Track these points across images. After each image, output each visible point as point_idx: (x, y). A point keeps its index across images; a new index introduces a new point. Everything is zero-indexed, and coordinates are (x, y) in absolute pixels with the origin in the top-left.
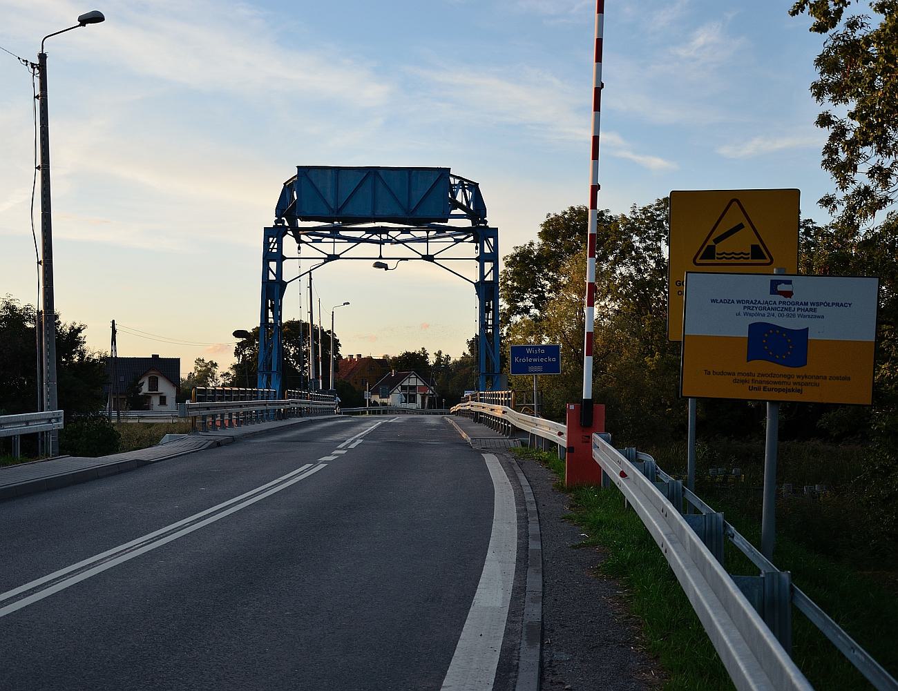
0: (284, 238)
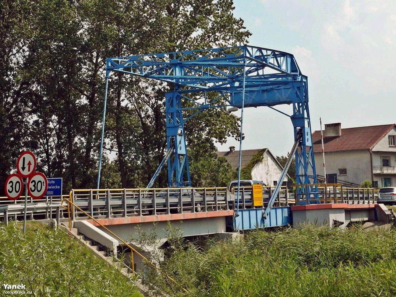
0: (383, 204)
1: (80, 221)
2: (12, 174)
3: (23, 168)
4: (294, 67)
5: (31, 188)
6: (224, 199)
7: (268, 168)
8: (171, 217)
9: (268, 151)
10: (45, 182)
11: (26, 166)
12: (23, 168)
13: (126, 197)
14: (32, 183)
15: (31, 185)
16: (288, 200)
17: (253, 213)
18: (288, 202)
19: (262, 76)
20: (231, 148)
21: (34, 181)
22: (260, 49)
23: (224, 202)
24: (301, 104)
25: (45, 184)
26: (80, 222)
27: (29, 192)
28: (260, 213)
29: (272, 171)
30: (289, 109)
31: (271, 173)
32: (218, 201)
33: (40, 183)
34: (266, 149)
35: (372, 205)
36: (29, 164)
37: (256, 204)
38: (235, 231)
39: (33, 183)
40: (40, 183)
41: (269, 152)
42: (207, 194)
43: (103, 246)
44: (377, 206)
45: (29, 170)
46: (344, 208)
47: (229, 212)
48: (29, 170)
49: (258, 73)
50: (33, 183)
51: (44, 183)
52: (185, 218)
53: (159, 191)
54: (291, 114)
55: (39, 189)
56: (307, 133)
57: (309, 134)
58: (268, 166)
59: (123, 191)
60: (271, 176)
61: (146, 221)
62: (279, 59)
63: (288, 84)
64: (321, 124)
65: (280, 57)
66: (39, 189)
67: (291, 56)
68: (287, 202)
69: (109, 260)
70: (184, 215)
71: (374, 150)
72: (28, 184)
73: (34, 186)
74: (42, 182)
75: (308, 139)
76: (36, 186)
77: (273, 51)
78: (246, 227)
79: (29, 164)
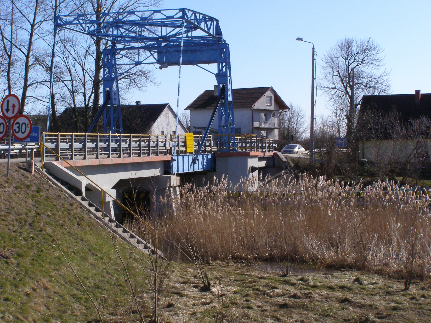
1: (51, 162)
2: (24, 115)
3: (8, 110)
4: (219, 32)
5: (15, 130)
6: (163, 145)
7: (169, 120)
8: (123, 160)
9: (169, 106)
10: (29, 124)
11: (11, 108)
12: (8, 110)
13: (87, 141)
14: (16, 124)
15: (15, 127)
16: (212, 148)
17: (186, 158)
18: (212, 150)
19: (190, 37)
20: (137, 102)
21: (18, 123)
22: (195, 13)
23: (164, 148)
24: (224, 64)
25: (29, 126)
26: (51, 162)
27: (13, 134)
28: (191, 158)
29: (171, 123)
30: (214, 67)
31: (171, 124)
32: (151, 147)
33: (24, 125)
34: (167, 104)
35: (271, 154)
36: (14, 106)
37: (189, 150)
38: (173, 175)
39: (18, 125)
40: (24, 125)
41: (170, 108)
42: (88, 140)
43: (72, 186)
44: (275, 154)
45: (13, 112)
46: (258, 156)
47: (168, 157)
48: (13, 112)
49: (187, 35)
50: (18, 125)
51: (28, 125)
52: (124, 162)
53: (103, 136)
54: (216, 72)
55: (23, 131)
56: (229, 89)
57: (230, 90)
58: (169, 118)
59: (71, 136)
60: (171, 127)
61: (103, 163)
62: (208, 22)
63: (214, 45)
64: (179, 87)
65: (209, 21)
66: (23, 131)
67: (217, 21)
68: (211, 150)
69: (79, 198)
70: (133, 159)
71: (255, 108)
72: (13, 125)
73: (18, 127)
74: (27, 124)
75: (229, 95)
76: (20, 127)
77: (204, 15)
78: (181, 171)
79: (14, 106)
